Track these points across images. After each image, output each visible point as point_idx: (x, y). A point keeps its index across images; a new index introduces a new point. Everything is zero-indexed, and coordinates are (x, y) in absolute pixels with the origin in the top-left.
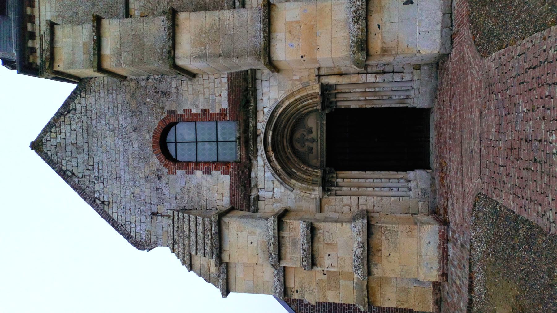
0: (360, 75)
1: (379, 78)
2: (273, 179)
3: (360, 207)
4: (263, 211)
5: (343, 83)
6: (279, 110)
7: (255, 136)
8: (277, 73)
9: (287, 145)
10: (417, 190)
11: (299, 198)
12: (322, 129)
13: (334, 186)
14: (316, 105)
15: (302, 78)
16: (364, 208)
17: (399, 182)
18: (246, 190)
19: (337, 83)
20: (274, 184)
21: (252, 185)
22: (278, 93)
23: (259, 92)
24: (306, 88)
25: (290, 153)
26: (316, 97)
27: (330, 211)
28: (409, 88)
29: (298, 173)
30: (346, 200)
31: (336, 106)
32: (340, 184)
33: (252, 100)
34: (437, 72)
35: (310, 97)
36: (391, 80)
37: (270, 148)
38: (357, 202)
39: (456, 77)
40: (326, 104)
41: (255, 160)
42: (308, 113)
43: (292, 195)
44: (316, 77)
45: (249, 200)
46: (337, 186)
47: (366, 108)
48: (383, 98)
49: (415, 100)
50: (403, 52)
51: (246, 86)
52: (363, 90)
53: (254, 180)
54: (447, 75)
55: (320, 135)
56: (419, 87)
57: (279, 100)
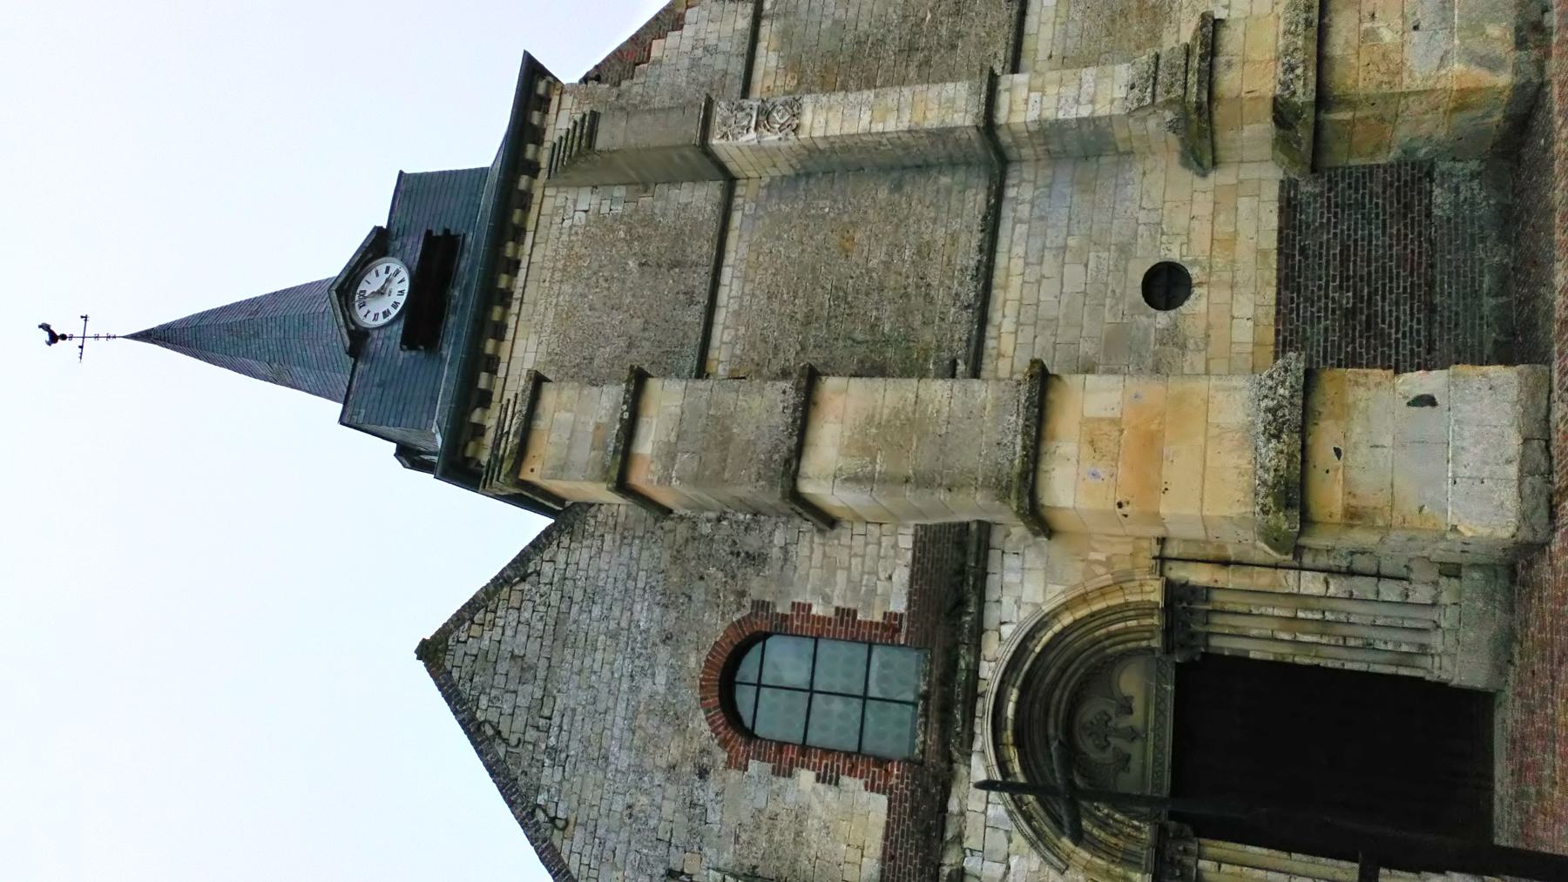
0: (1279, 571)
2: (1010, 826)
5: (1230, 586)
6: (1042, 633)
8: (1045, 539)
12: (1162, 707)
14: (1148, 635)
20: (1010, 841)
23: (993, 580)
28: (1428, 625)
34: (1509, 589)
35: (1132, 613)
36: (1371, 596)
37: (1008, 736)
41: (965, 765)
44: (1153, 562)
55: (1156, 720)
56: (1457, 625)
57: (1046, 609)
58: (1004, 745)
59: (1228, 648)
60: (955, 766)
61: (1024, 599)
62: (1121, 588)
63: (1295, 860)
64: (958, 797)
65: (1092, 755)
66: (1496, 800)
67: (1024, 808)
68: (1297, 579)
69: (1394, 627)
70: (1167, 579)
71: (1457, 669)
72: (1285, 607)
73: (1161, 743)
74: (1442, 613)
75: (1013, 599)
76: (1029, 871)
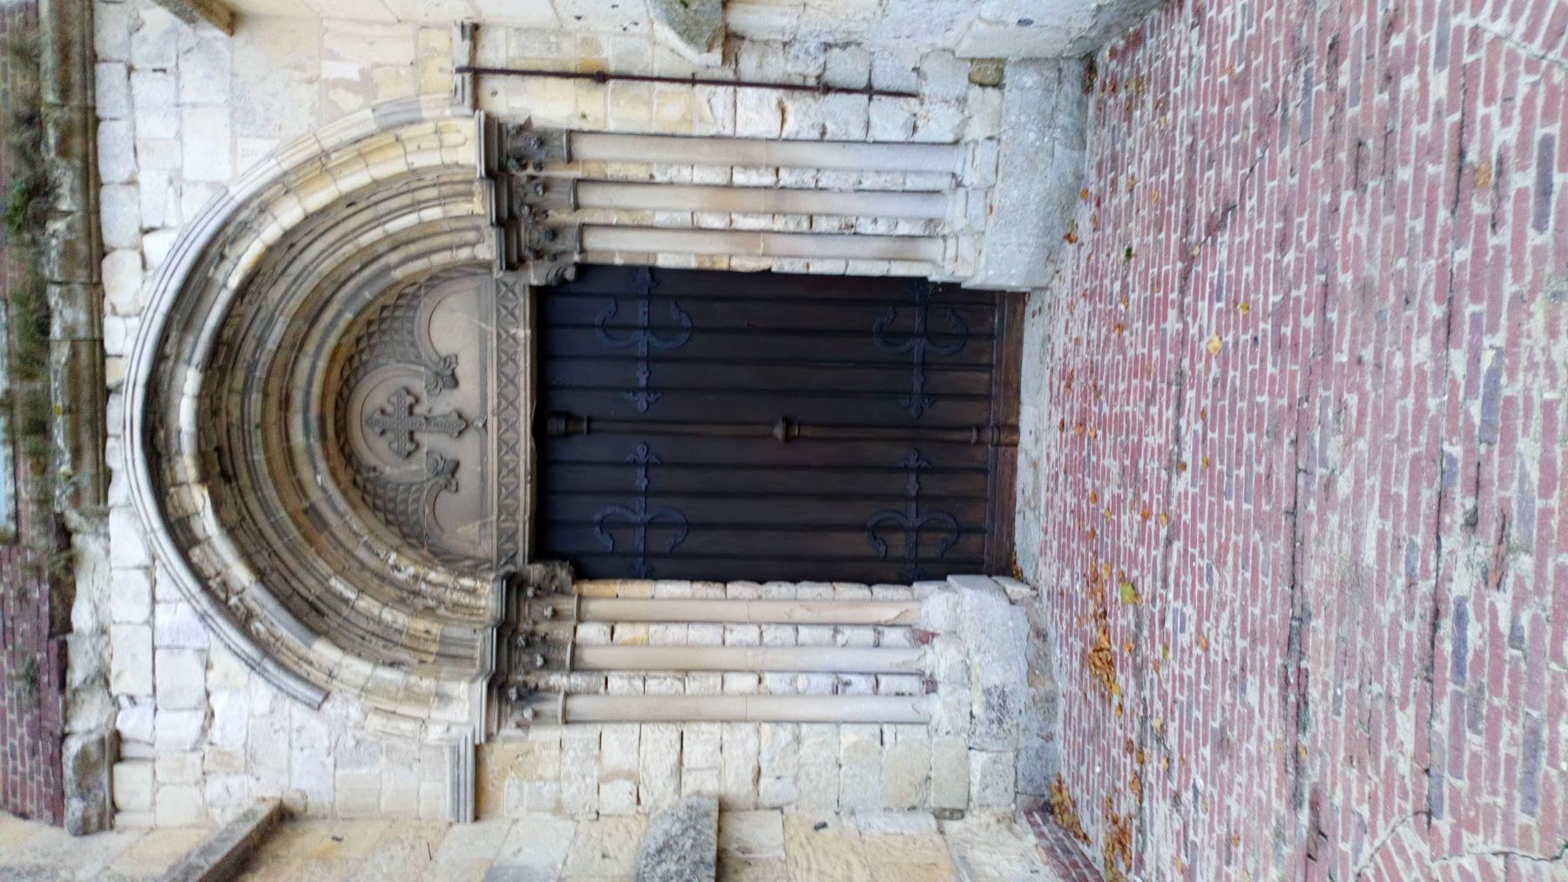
0: (698, 87)
1: (803, 114)
2: (204, 638)
3: (691, 783)
4: (146, 820)
5: (612, 126)
6: (240, 247)
7: (86, 394)
8: (220, 34)
9: (309, 448)
10: (964, 695)
11: (358, 742)
12: (509, 369)
13: (560, 667)
14: (471, 236)
15: (377, 74)
16: (711, 786)
17: (877, 645)
18: (39, 704)
19: (576, 124)
20: (208, 666)
21: (76, 676)
23: (112, 137)
24: (406, 133)
25: (323, 489)
26: (469, 195)
27: (530, 810)
28: (944, 183)
29: (365, 603)
30: (618, 745)
31: (582, 251)
32: (590, 656)
33: (66, 180)
34: (1082, 105)
35: (433, 192)
36: (857, 134)
37: (186, 466)
38: (674, 758)
39: (1248, 103)
41: (97, 533)
42: (436, 280)
43: (317, 728)
44: (458, 77)
45: (56, 761)
46: (574, 668)
47: (731, 275)
48: (816, 228)
49: (966, 245)
50: (642, 673)
51: (30, 92)
52: (719, 178)
53: (88, 646)
54: (1162, 106)
55: (500, 395)
56: (991, 178)
57: (240, 193)
58: (181, 484)
59: (621, 252)
60: (77, 540)
61: (189, 174)
62: (397, 139)
63: (735, 599)
64: (90, 600)
65: (388, 469)
66: (1022, 461)
67: (233, 601)
68: (730, 106)
69: (890, 191)
70: (488, 118)
71: (983, 260)
72: (712, 165)
75: (165, 176)
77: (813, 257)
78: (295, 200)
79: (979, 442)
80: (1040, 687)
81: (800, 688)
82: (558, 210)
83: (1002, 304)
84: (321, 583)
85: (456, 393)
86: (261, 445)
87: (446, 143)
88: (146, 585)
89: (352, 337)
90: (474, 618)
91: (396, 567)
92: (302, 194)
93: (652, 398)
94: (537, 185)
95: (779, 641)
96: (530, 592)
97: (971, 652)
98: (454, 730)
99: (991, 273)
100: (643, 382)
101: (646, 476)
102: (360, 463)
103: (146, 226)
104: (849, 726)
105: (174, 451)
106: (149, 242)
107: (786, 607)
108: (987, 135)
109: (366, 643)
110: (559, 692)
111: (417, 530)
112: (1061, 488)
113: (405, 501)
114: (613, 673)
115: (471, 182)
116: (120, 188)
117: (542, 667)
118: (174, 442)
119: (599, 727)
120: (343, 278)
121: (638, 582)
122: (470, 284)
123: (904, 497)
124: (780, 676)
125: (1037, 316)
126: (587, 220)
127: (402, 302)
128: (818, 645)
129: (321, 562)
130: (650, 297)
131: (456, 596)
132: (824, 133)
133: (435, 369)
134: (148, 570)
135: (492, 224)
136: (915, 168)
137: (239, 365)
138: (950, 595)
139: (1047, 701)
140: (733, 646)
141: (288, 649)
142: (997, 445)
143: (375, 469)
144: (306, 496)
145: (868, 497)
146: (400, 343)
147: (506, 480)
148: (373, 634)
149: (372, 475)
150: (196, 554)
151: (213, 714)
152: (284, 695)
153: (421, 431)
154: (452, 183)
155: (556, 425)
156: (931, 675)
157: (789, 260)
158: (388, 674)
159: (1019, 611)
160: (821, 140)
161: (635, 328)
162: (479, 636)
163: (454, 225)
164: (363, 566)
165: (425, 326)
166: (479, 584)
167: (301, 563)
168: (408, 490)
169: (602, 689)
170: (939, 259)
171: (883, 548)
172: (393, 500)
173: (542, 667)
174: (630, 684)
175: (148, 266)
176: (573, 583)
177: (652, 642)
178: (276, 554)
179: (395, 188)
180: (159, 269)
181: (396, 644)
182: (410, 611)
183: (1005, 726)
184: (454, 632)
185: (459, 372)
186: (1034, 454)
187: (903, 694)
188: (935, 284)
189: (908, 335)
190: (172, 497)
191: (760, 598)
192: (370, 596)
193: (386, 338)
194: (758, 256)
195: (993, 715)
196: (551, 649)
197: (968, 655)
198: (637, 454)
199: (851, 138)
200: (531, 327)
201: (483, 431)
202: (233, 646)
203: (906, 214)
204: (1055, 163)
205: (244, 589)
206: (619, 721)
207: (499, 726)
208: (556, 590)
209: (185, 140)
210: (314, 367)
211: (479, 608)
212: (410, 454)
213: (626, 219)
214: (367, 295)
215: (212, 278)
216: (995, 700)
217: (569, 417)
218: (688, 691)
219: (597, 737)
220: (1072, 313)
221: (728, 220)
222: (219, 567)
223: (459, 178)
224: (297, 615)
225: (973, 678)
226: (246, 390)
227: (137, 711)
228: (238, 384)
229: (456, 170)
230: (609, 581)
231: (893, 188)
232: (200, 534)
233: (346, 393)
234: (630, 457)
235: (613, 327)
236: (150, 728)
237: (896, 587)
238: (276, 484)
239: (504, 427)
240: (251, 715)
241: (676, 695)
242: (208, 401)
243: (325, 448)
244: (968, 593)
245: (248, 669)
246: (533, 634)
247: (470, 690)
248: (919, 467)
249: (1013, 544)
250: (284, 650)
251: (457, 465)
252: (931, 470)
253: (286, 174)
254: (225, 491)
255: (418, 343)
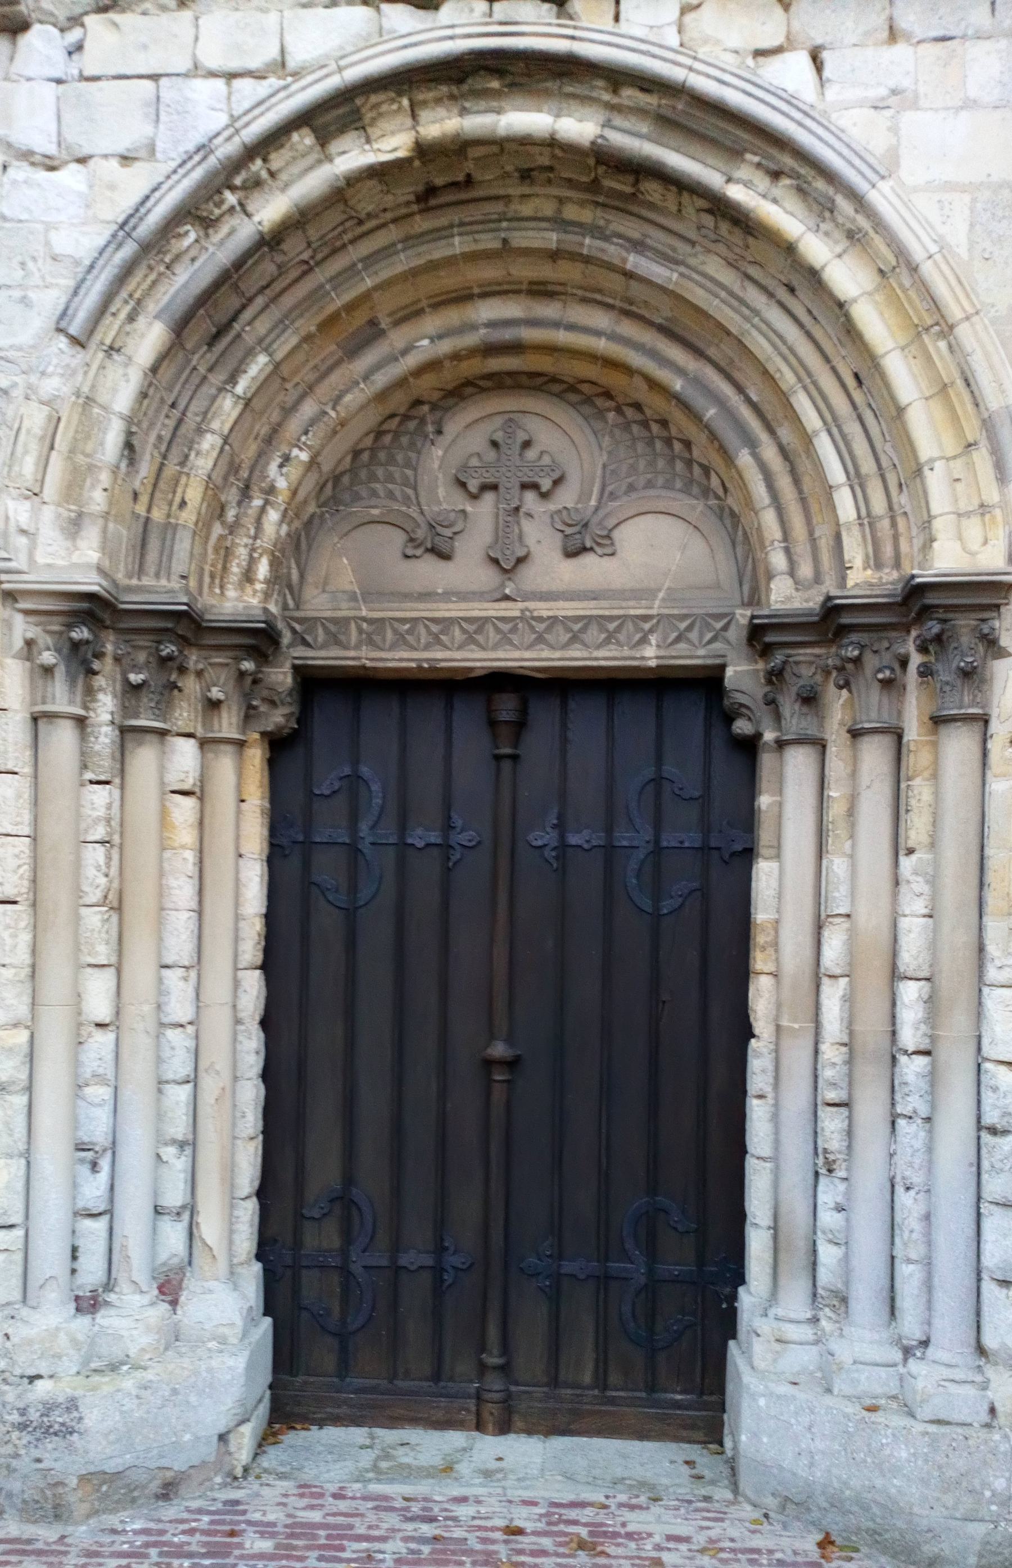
6: (792, 202)
9: (473, 327)
10: (69, 1365)
14: (806, 570)
17: (158, 1211)
20: (126, 159)
22: (949, 186)
24: (982, 458)
26: (877, 563)
28: (910, 1326)
29: (228, 409)
31: (781, 745)
35: (879, 505)
40: (804, 654)
46: (124, 731)
48: (824, 1113)
50: (116, 839)
55: (554, 619)
56: (926, 1412)
61: (908, 118)
63: (236, 984)
66: (455, 1439)
67: (231, 198)
72: (933, 946)
73: (493, 636)
74: (959, 1375)
75: (906, 83)
76: (49, 227)
77: (776, 1105)
78: (869, 287)
79: (483, 1368)
80: (80, 1493)
81: (88, 1091)
82: (850, 703)
83: (705, 1406)
84: (260, 341)
85: (557, 555)
86: (474, 247)
87: (964, 522)
88: (254, 63)
89: (641, 392)
90: (207, 579)
91: (286, 459)
92: (879, 298)
93: (550, 854)
94: (892, 670)
95: (166, 1053)
96: (248, 665)
97: (139, 1374)
98: (23, 541)
99: (762, 1402)
100: (573, 839)
101: (428, 845)
102: (447, 409)
103: (825, 55)
104: (22, 1171)
105: (467, 105)
106: (799, 61)
107: (222, 1065)
108: (998, 1406)
109: (166, 408)
110: (86, 708)
111: (346, 497)
112: (410, 1526)
113: (390, 478)
114: (117, 793)
115: (897, 565)
116: (884, 16)
117: (126, 681)
118: (483, 104)
119: (27, 770)
120: (737, 375)
121: (266, 832)
122: (726, 572)
123: (396, 1248)
124: (110, 1057)
125: (685, 1470)
126: (832, 750)
127: (697, 470)
128: (160, 1116)
129: (294, 341)
130: (705, 850)
131: (242, 552)
132: (993, 1131)
133: (595, 521)
134: (280, 66)
135: (829, 598)
136: (936, 1281)
137: (599, 212)
138: (239, 1330)
139: (56, 1507)
140: (160, 980)
141: (154, 283)
142: (479, 1397)
143: (439, 432)
144: (397, 323)
145: (397, 1191)
146: (633, 469)
147: (423, 631)
148: (180, 422)
149: (430, 428)
150: (304, 139)
151: (52, 169)
152: (80, 276)
153: (498, 502)
154: (896, 538)
155: (506, 707)
156: (107, 1303)
157: (770, 1067)
158: (113, 438)
159: (209, 1451)
160: (979, 1127)
161: (658, 827)
162: (175, 584)
163: (825, 544)
164: (288, 411)
165: (661, 506)
166: (259, 586)
167: (291, 310)
168: (406, 483)
169: (89, 776)
170: (780, 1312)
171: (316, 1213)
172: (391, 460)
173: (126, 681)
174: (98, 819)
175: (761, 60)
176: (263, 734)
177: (167, 854)
178: (305, 274)
179: (887, 451)
180: (758, 76)
181: (165, 457)
182: (217, 477)
183: (15, 1435)
184: (183, 545)
185: (588, 560)
186: (464, 1468)
187: (74, 1258)
188: (734, 1297)
189: (652, 1253)
190: (393, 101)
191: (238, 1022)
192: (241, 415)
193: (640, 447)
194: (777, 1018)
195: (34, 1415)
196: (156, 697)
197: (136, 1367)
198: (462, 831)
199: (985, 1177)
200: (658, 667)
201: (498, 596)
202: (157, 194)
203: (855, 1262)
204: (955, 1523)
205: (249, 215)
206: (36, 802)
207: (27, 612)
208: (250, 707)
209: (964, 114)
210: (598, 333)
211: (222, 587)
212: (463, 485)
213: (836, 810)
214: (711, 413)
215: (743, 160)
216: (58, 1418)
217: (520, 726)
218: (84, 911)
219: (10, 766)
220: (703, 1551)
221: (838, 971)
222: (284, 177)
223: (904, 546)
224: (207, 297)
225: (96, 1378)
226: (559, 223)
227: (60, 56)
228: (571, 212)
229: (917, 543)
230: (267, 790)
231: (897, 1240)
232: (335, 146)
233: (556, 388)
234: (458, 822)
235: (658, 795)
236: (31, 74)
237: (255, 1237)
238: (414, 273)
239: (505, 627)
240: (49, 227)
241: (78, 892)
242: (545, 161)
243: (473, 352)
244: (239, 1363)
245: (120, 220)
246: (182, 670)
247: (88, 566)
248: (443, 1270)
249: (321, 1424)
250: (153, 277)
251: (445, 556)
252: (438, 1289)
253: (914, 269)
254: (404, 193)
255: (634, 495)
